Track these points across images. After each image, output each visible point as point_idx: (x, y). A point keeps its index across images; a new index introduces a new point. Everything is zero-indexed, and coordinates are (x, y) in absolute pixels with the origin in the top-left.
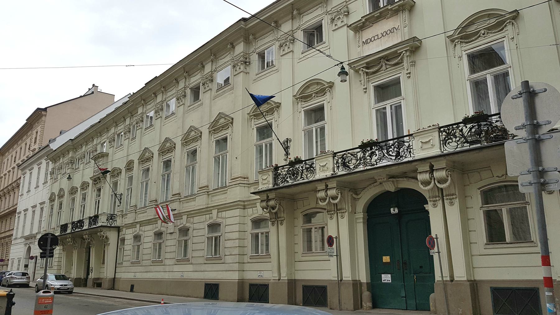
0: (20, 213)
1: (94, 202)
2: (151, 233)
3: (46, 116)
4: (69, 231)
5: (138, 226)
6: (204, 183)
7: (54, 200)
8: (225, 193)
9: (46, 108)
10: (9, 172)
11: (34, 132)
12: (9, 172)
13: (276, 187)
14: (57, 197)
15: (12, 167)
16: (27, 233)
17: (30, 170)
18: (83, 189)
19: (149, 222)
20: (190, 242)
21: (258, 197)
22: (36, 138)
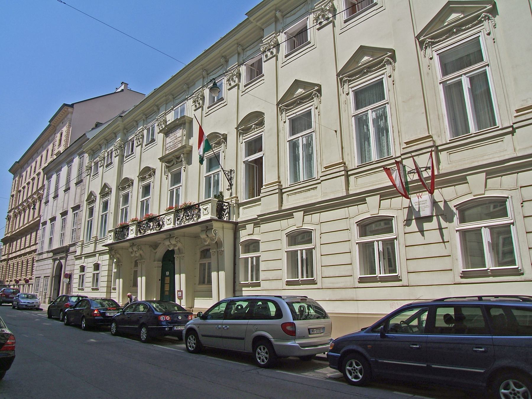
0: (45, 223)
1: (286, 149)
2: (92, 265)
3: (72, 113)
4: (132, 235)
5: (97, 255)
6: (133, 217)
7: (94, 201)
8: (313, 189)
9: (73, 105)
10: (28, 184)
11: (58, 135)
12: (28, 184)
13: (139, 235)
14: (85, 203)
15: (32, 177)
16: (56, 245)
17: (57, 172)
18: (142, 178)
19: (88, 256)
20: (316, 255)
21: (107, 248)
22: (60, 140)
